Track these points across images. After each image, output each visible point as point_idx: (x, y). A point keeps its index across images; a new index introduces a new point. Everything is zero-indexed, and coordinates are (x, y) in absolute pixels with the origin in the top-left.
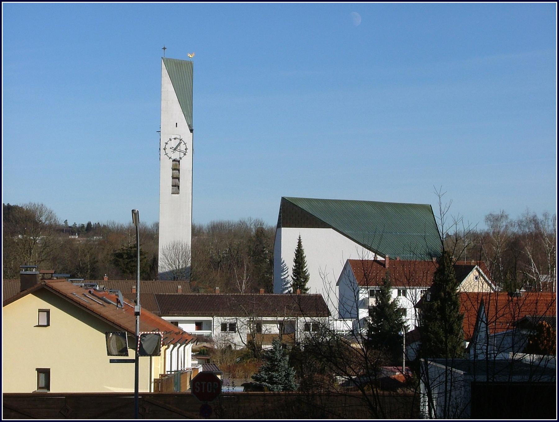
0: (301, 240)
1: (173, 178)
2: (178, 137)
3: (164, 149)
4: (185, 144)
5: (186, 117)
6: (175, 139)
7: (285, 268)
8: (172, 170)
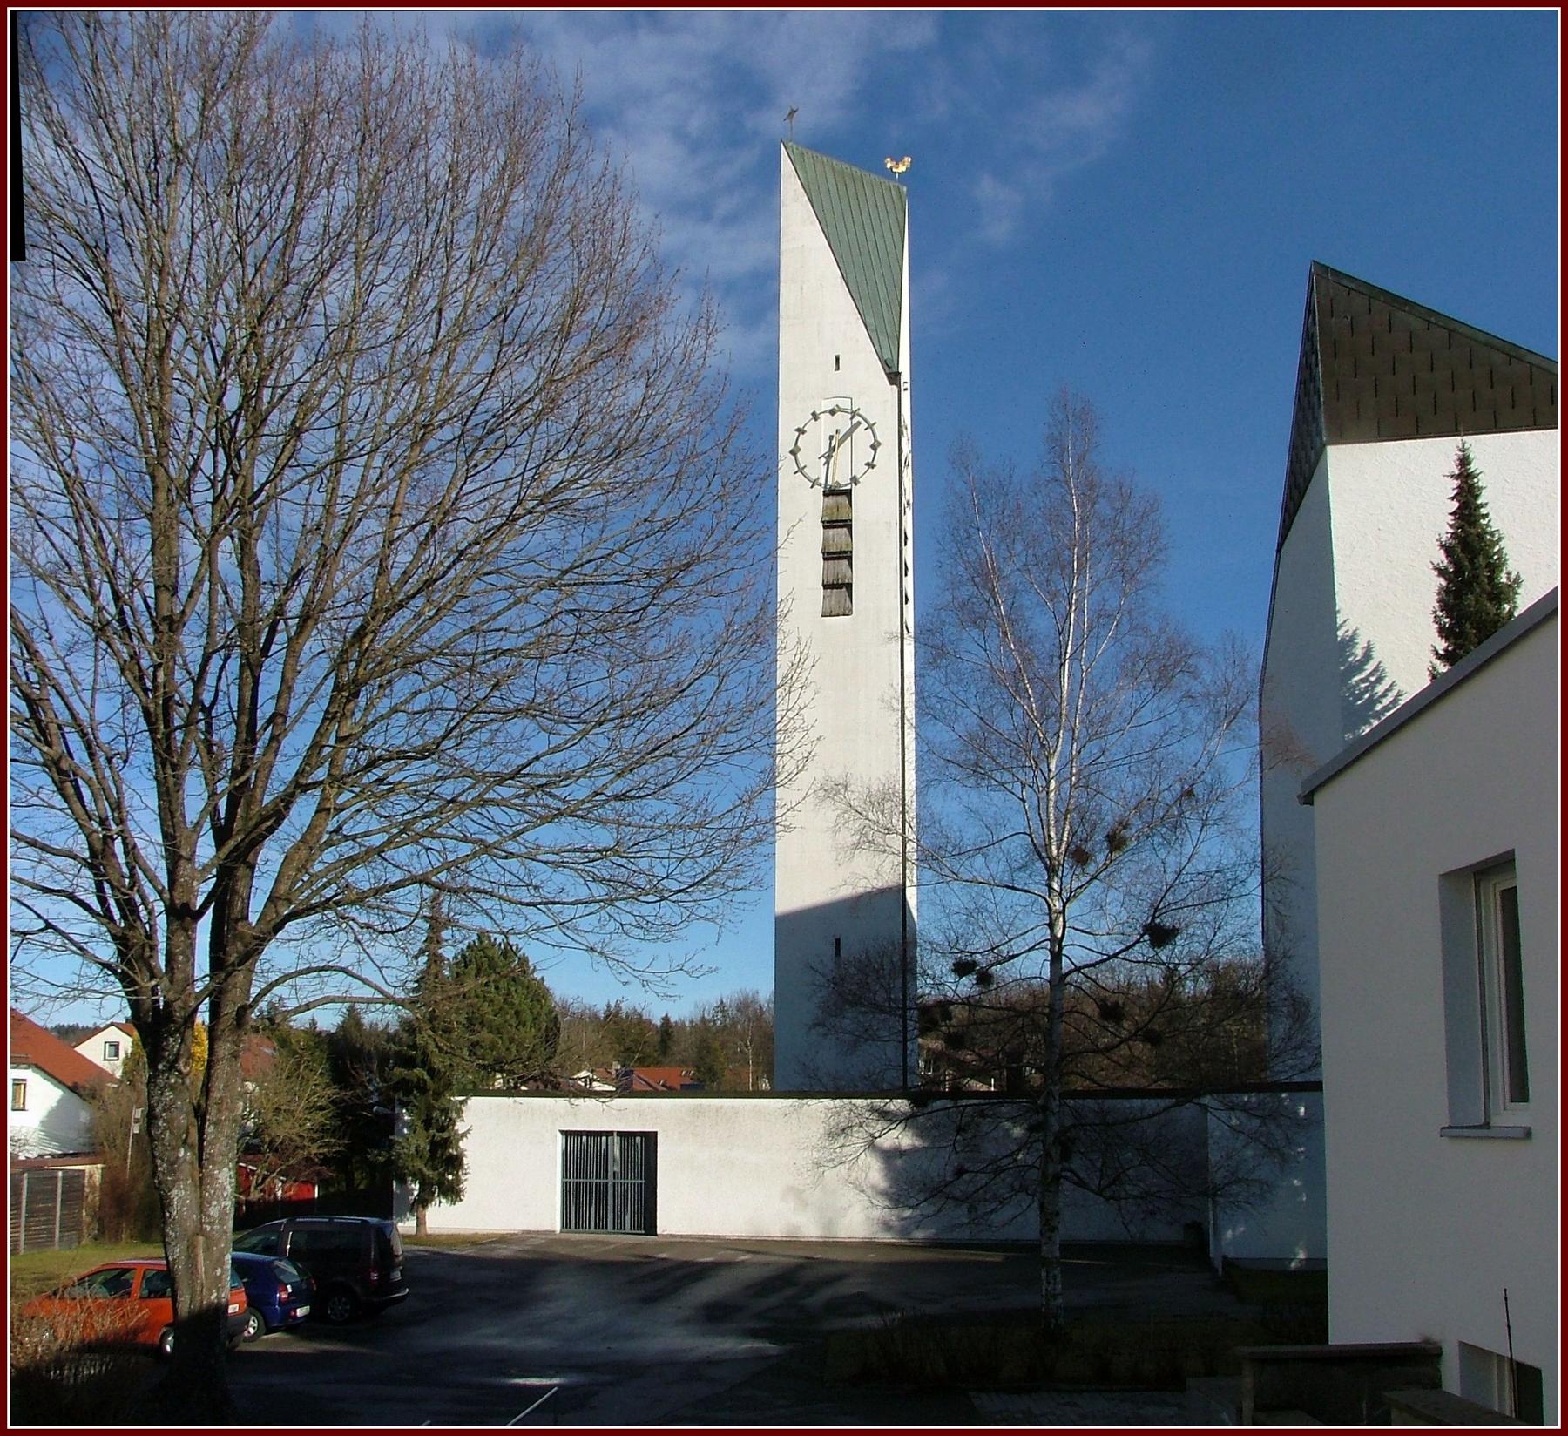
0: (1471, 476)
1: (829, 556)
2: (845, 404)
3: (793, 453)
4: (870, 426)
5: (874, 335)
6: (832, 412)
7: (1380, 689)
8: (824, 527)
